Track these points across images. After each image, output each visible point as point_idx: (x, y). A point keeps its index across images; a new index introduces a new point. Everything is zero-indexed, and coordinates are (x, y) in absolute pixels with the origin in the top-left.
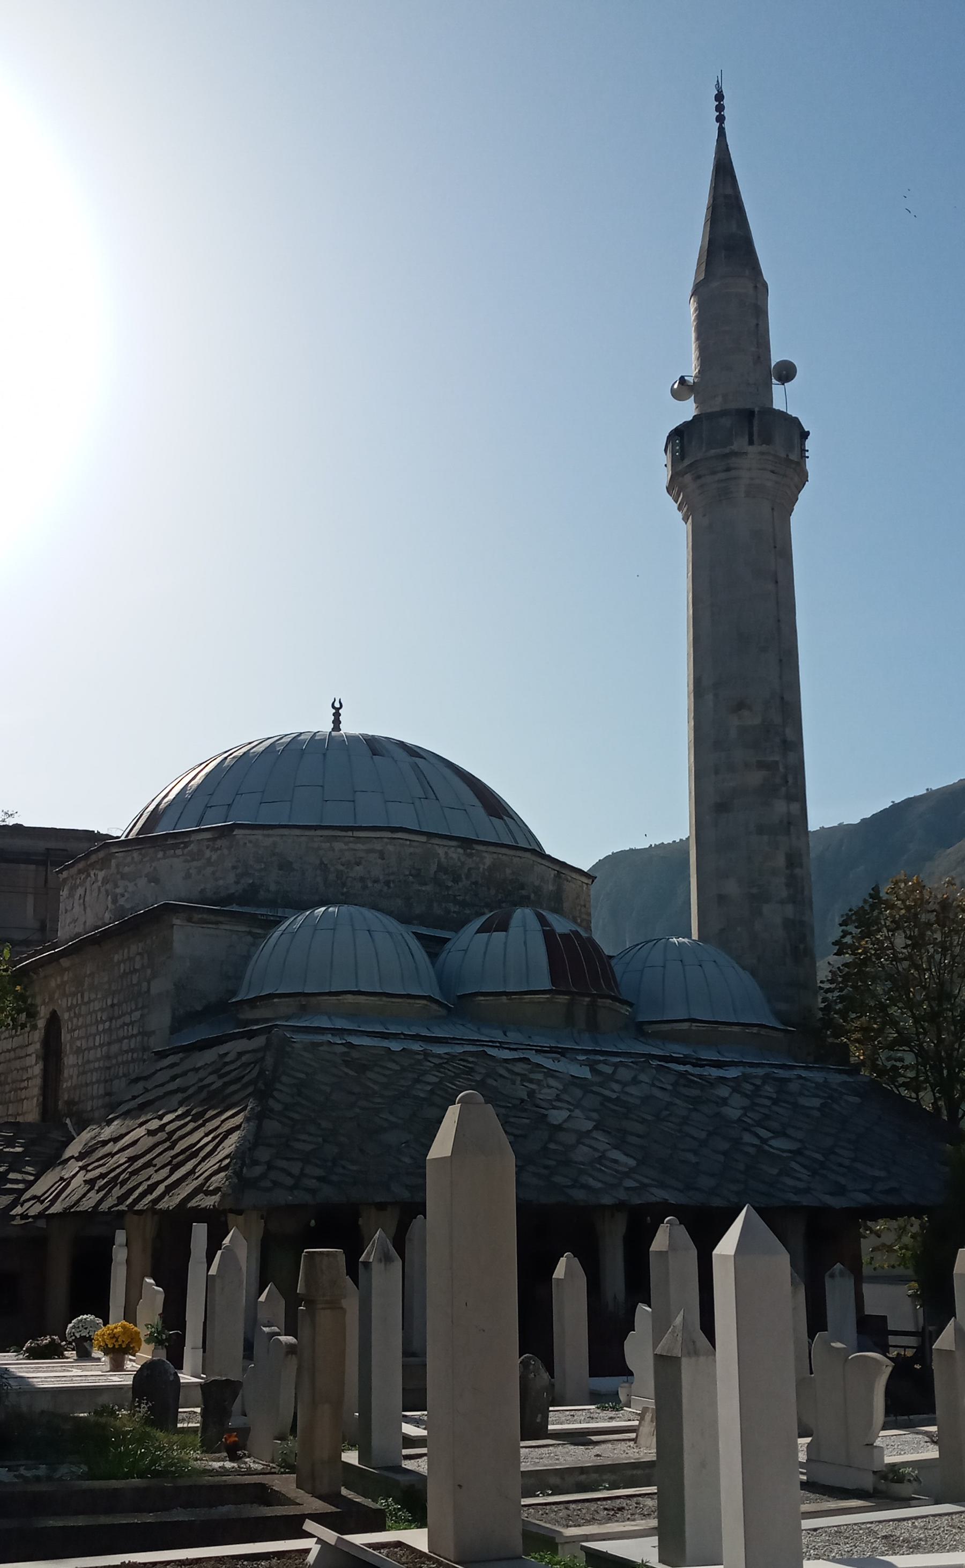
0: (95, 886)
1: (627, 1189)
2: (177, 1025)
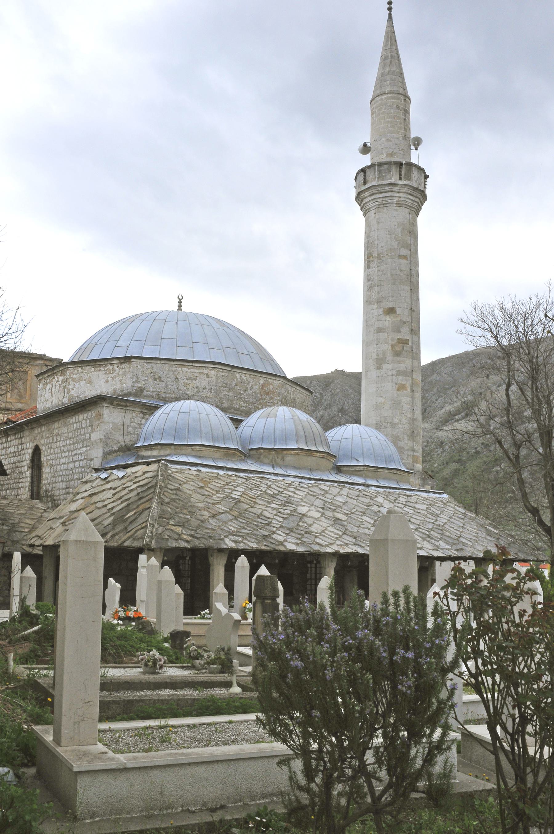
0: (58, 384)
1: (338, 545)
2: (106, 455)
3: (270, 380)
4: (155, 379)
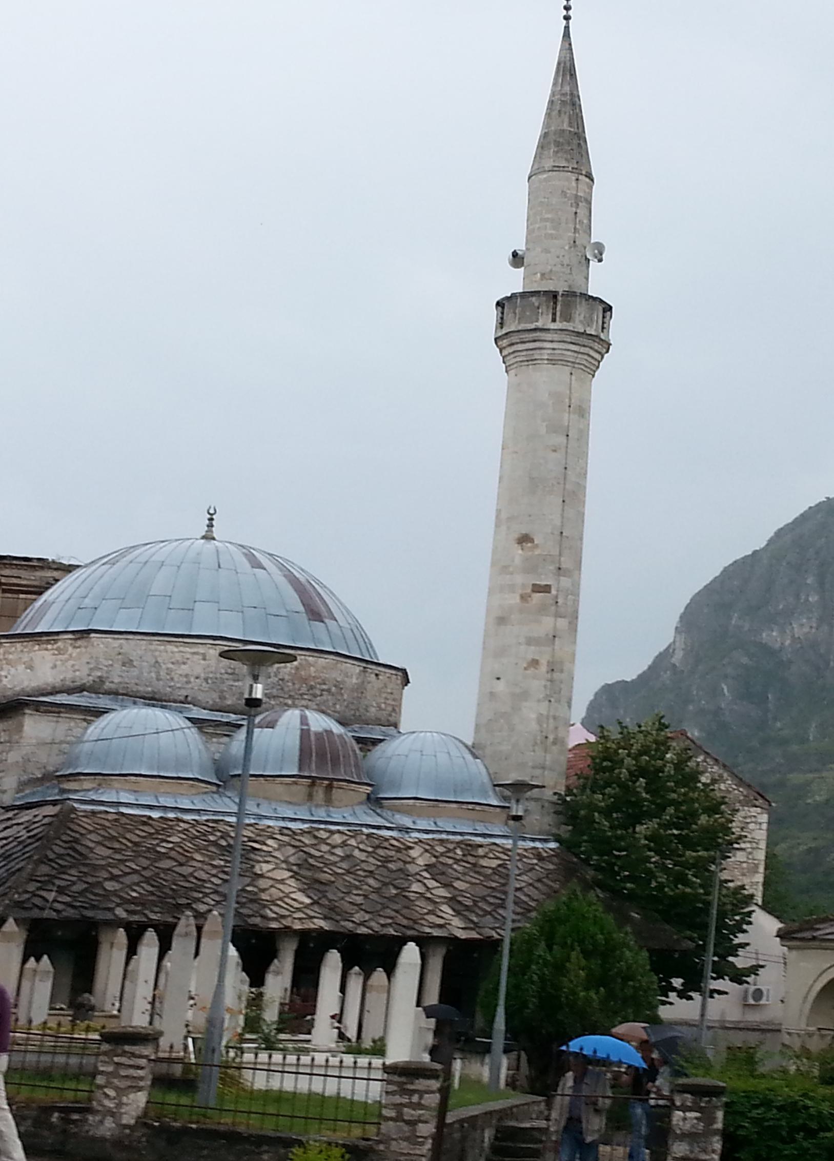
2: (22, 786)
3: (311, 658)
4: (124, 665)
